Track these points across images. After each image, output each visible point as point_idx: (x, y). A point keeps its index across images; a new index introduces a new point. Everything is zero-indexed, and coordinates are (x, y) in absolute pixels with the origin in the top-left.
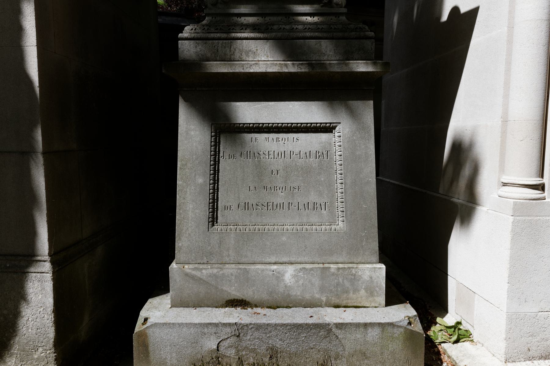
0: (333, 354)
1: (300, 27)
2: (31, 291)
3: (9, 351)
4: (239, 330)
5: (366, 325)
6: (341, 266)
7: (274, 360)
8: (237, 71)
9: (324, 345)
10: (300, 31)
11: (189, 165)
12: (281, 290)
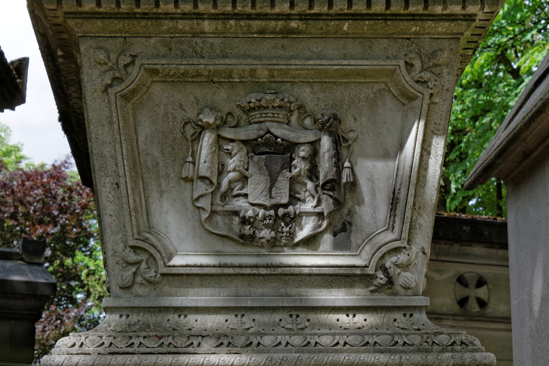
1: (326, 340)
10: (326, 350)
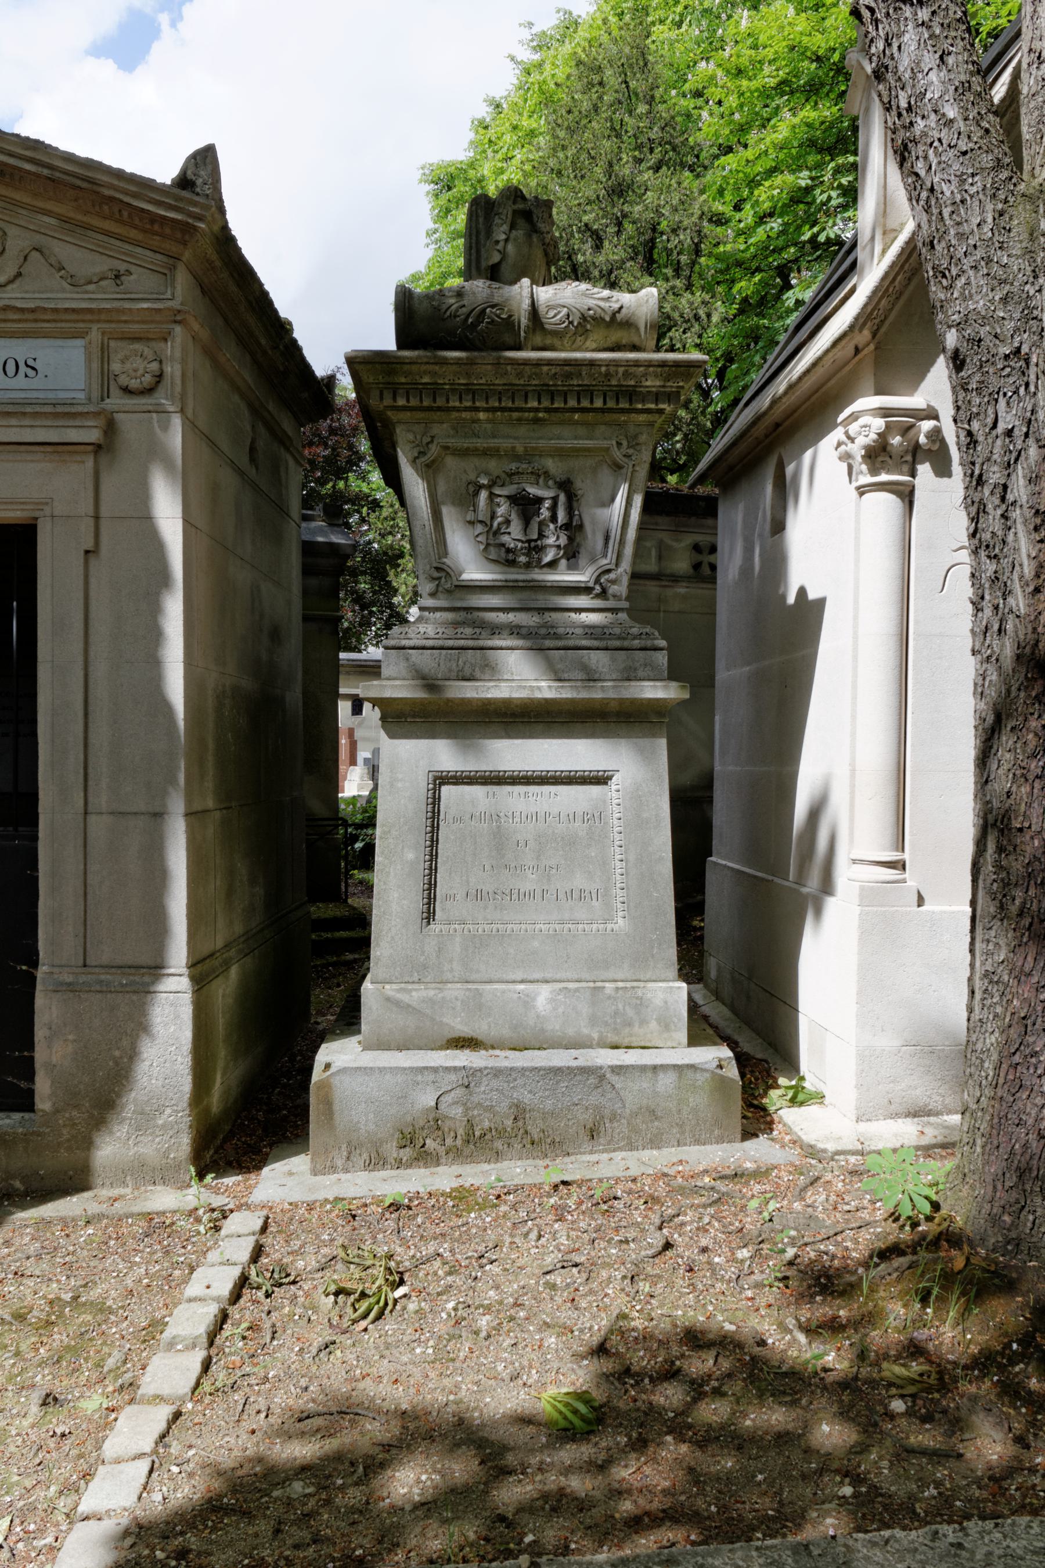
0: (607, 1112)
2: (159, 1020)
3: (119, 1114)
4: (469, 1079)
5: (655, 1068)
6: (620, 984)
7: (520, 1123)
8: (468, 695)
9: (594, 1099)
11: (394, 833)
12: (531, 1023)
